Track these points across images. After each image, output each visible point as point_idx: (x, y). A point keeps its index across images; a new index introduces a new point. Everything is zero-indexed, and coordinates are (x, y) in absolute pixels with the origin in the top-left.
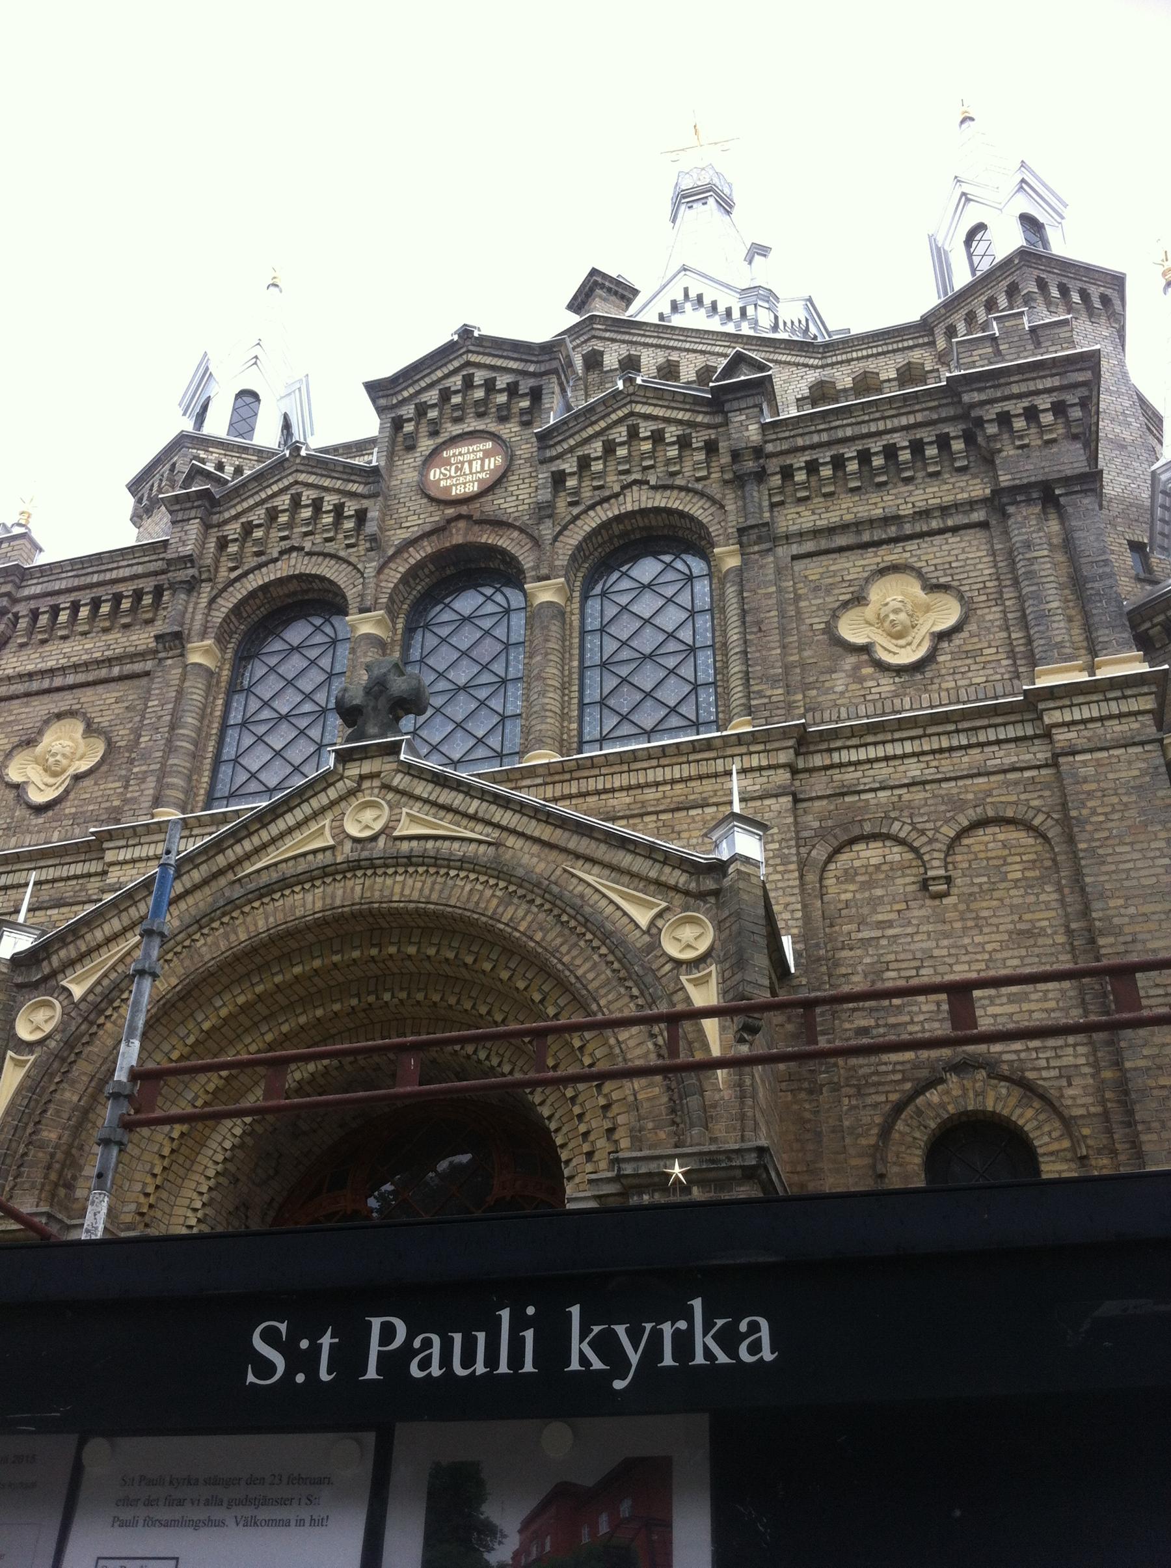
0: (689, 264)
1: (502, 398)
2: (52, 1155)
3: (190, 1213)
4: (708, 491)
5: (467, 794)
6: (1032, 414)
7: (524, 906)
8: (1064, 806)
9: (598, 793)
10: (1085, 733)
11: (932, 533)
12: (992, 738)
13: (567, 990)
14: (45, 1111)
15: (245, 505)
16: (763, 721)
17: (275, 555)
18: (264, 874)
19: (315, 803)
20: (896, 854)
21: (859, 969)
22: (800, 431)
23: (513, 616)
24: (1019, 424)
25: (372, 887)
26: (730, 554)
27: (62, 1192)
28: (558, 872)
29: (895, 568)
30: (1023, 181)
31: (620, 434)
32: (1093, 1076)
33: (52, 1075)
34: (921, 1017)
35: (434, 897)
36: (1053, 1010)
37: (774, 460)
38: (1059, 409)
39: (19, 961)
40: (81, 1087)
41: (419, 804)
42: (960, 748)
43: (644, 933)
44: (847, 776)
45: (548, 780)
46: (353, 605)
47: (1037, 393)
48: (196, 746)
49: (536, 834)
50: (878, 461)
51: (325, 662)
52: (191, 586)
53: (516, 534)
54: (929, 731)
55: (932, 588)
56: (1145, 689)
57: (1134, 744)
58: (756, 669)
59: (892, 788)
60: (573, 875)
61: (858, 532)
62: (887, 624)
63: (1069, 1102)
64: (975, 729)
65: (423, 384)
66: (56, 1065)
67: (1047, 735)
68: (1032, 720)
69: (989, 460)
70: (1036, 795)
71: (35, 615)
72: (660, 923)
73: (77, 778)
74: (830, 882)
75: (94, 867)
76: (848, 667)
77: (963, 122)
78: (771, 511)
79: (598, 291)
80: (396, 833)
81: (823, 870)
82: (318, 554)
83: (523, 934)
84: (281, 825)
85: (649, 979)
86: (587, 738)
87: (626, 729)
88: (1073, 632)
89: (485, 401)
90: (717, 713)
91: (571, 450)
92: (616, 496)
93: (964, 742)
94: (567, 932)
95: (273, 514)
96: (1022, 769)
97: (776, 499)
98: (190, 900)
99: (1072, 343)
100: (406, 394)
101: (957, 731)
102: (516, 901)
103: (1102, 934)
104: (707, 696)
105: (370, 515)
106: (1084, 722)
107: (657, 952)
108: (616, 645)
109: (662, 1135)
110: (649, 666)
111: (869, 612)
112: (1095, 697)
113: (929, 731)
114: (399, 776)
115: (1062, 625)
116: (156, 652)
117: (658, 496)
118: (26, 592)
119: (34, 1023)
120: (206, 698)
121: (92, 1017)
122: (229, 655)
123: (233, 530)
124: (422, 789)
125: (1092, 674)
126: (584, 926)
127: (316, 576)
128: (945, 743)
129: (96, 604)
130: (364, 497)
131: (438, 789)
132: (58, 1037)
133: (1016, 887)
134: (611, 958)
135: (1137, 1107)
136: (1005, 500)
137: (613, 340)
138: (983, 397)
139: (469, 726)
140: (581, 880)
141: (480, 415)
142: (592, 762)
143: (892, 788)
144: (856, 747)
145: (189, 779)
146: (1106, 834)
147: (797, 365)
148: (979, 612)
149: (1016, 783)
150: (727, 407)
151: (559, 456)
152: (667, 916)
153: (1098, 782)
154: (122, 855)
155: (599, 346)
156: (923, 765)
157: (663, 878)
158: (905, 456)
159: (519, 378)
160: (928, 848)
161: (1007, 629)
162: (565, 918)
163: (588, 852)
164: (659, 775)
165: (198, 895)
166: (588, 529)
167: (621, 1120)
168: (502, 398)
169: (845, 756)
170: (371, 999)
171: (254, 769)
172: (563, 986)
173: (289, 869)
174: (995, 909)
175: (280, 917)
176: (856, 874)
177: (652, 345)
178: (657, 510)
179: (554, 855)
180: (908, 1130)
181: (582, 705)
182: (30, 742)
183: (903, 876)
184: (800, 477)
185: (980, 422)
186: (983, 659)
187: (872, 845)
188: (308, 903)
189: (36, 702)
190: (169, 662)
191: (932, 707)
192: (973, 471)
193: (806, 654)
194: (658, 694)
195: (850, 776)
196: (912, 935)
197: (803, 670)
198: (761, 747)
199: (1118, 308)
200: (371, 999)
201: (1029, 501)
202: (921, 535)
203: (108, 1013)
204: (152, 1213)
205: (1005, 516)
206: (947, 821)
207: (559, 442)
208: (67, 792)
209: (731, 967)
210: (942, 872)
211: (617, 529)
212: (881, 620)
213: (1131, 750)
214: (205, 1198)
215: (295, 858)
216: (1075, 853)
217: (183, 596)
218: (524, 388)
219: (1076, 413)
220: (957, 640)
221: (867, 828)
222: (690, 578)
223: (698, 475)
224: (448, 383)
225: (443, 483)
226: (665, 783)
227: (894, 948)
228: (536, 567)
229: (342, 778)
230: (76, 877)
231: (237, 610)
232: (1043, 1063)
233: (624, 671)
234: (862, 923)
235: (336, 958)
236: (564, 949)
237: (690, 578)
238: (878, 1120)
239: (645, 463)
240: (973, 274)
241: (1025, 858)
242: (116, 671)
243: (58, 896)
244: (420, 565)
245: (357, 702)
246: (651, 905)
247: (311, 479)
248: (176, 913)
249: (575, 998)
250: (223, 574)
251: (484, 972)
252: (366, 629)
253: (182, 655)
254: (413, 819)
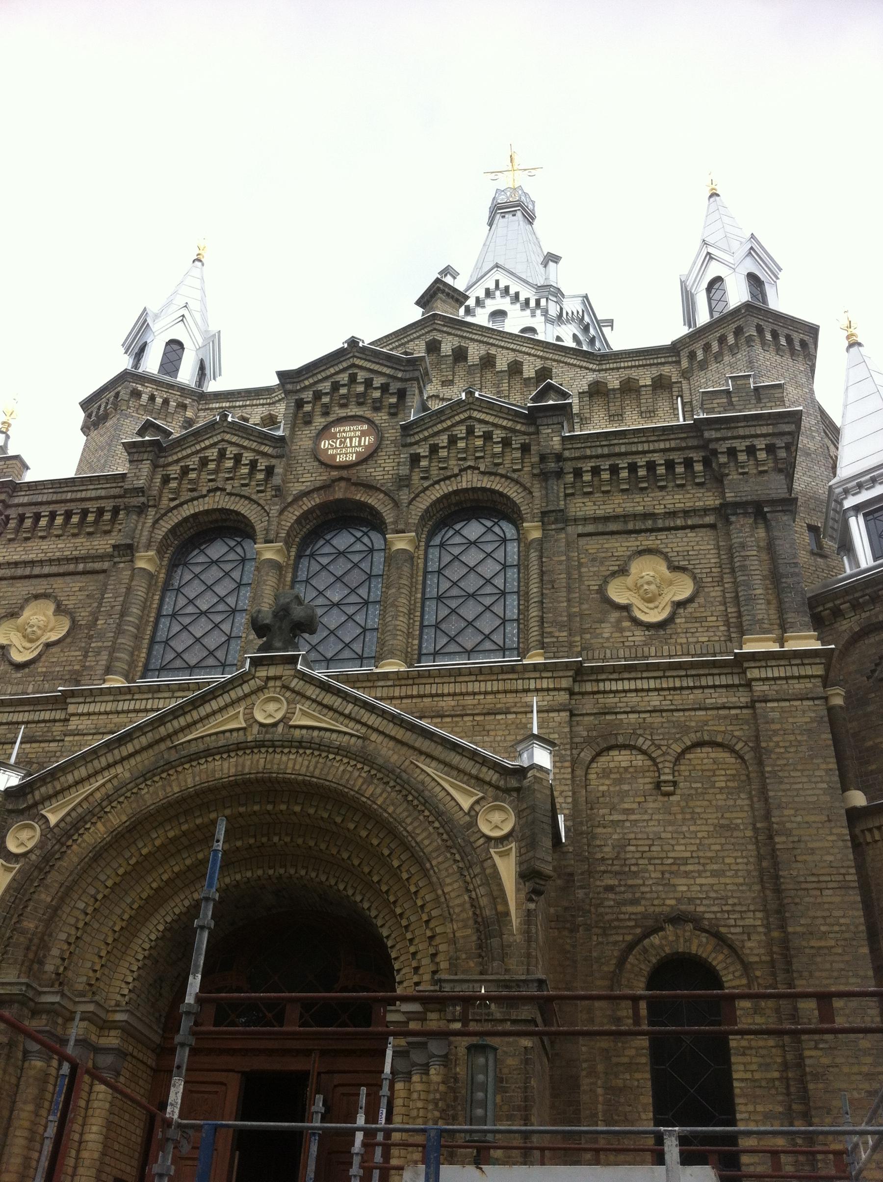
0: (500, 263)
1: (377, 394)
2: (31, 940)
3: (124, 985)
4: (522, 480)
5: (344, 699)
6: (751, 451)
7: (382, 786)
8: (757, 737)
9: (432, 696)
10: (775, 687)
11: (676, 528)
12: (710, 683)
13: (408, 849)
14: (26, 907)
15: (184, 453)
16: (552, 655)
17: (205, 492)
18: (193, 744)
19: (233, 694)
20: (639, 760)
21: (609, 842)
22: (589, 444)
23: (375, 554)
24: (742, 457)
25: (272, 761)
26: (535, 528)
27: (36, 966)
28: (407, 763)
29: (649, 551)
30: (752, 248)
31: (461, 431)
32: (765, 934)
33: (32, 881)
34: (651, 882)
35: (317, 773)
36: (742, 885)
37: (569, 463)
38: (771, 449)
39: (9, 793)
40: (53, 891)
41: (308, 703)
42: (688, 688)
43: (466, 814)
44: (608, 700)
45: (397, 683)
46: (260, 536)
47: (757, 436)
48: (138, 629)
49: (393, 734)
50: (642, 472)
51: (236, 575)
52: (141, 510)
53: (382, 496)
54: (668, 674)
55: (674, 568)
56: (818, 660)
57: (808, 699)
58: (549, 616)
59: (639, 712)
60: (417, 767)
61: (625, 522)
62: (641, 591)
63: (748, 951)
64: (699, 675)
65: (320, 377)
66: (36, 873)
67: (748, 685)
68: (739, 673)
69: (719, 480)
70: (738, 727)
71: (22, 518)
72: (477, 808)
73: (48, 645)
74: (592, 776)
75: (59, 715)
76: (612, 620)
77: (711, 196)
78: (565, 500)
79: (440, 295)
80: (291, 723)
81: (588, 768)
82: (236, 495)
83: (380, 806)
84: (207, 709)
85: (468, 849)
86: (424, 651)
87: (453, 648)
88: (771, 612)
89: (364, 395)
90: (519, 642)
91: (425, 439)
92: (456, 476)
93: (691, 684)
94: (411, 808)
95: (204, 462)
96: (730, 708)
97: (569, 491)
98: (138, 758)
99: (782, 402)
100: (307, 383)
101: (687, 676)
102: (375, 781)
103: (778, 834)
104: (512, 629)
105: (276, 470)
106: (774, 679)
107: (474, 829)
108: (448, 584)
109: (472, 964)
110: (471, 602)
111: (629, 581)
112: (782, 662)
113: (667, 674)
114: (296, 680)
115: (763, 607)
116: (112, 556)
117: (486, 479)
118: (16, 501)
119: (21, 840)
120: (147, 594)
121: (63, 839)
122: (165, 563)
123: (174, 470)
124: (311, 691)
125: (782, 641)
126: (424, 805)
127: (233, 511)
128: (678, 684)
129: (68, 515)
130: (273, 457)
131: (324, 693)
132: (38, 852)
133: (721, 793)
134: (441, 830)
135: (794, 960)
136: (729, 511)
137: (449, 334)
138: (718, 435)
139: (339, 633)
140: (423, 770)
141: (360, 404)
142: (429, 674)
143: (639, 712)
144: (616, 680)
145: (132, 654)
146: (784, 762)
147: (581, 367)
148: (706, 590)
149: (725, 717)
150: (539, 421)
151: (417, 443)
152: (483, 803)
153: (781, 723)
154: (82, 709)
155: (438, 336)
156: (661, 698)
157: (481, 776)
158: (661, 470)
159: (390, 380)
160: (662, 759)
161: (725, 604)
162: (410, 798)
163: (428, 751)
164: (476, 687)
165: (145, 755)
166: (434, 498)
167: (442, 948)
168: (377, 394)
169: (608, 686)
170: (264, 840)
171: (180, 650)
172: (405, 846)
173: (211, 743)
174: (705, 807)
175: (204, 777)
176: (611, 772)
177: (477, 341)
178: (484, 490)
179: (404, 750)
180: (636, 962)
181: (422, 627)
182: (13, 615)
183: (644, 777)
184: (587, 477)
185: (715, 453)
186: (706, 624)
187: (623, 752)
188: (225, 768)
189: (19, 584)
190: (122, 565)
191: (670, 656)
192: (708, 486)
193: (585, 606)
194: (477, 624)
195: (611, 700)
196: (647, 821)
197: (581, 618)
198: (550, 674)
199: (812, 351)
200: (264, 840)
201: (745, 514)
202: (669, 529)
203: (75, 837)
204: (97, 984)
205: (728, 523)
206: (676, 740)
207: (417, 433)
208: (40, 655)
209: (526, 846)
210: (670, 778)
211: (454, 499)
212: (637, 588)
213: (805, 703)
214: (135, 975)
215: (216, 734)
216: (762, 773)
217: (134, 517)
218: (393, 388)
219: (782, 454)
220: (690, 608)
221: (621, 740)
222: (504, 540)
223: (515, 467)
224: (338, 378)
225: (330, 452)
226: (480, 693)
227: (635, 829)
228: (395, 523)
229: (254, 678)
230: (44, 721)
231: (173, 531)
232: (732, 922)
233: (453, 604)
234: (613, 808)
235: (242, 809)
236: (409, 821)
237: (504, 540)
238: (616, 954)
239: (478, 454)
240: (711, 315)
241: (728, 772)
242: (81, 567)
243: (31, 734)
244: (311, 511)
245: (267, 621)
246: (471, 794)
247: (234, 439)
248: (127, 767)
249: (413, 856)
250: (165, 502)
251: (348, 829)
252: (268, 555)
253: (132, 561)
254: (304, 713)
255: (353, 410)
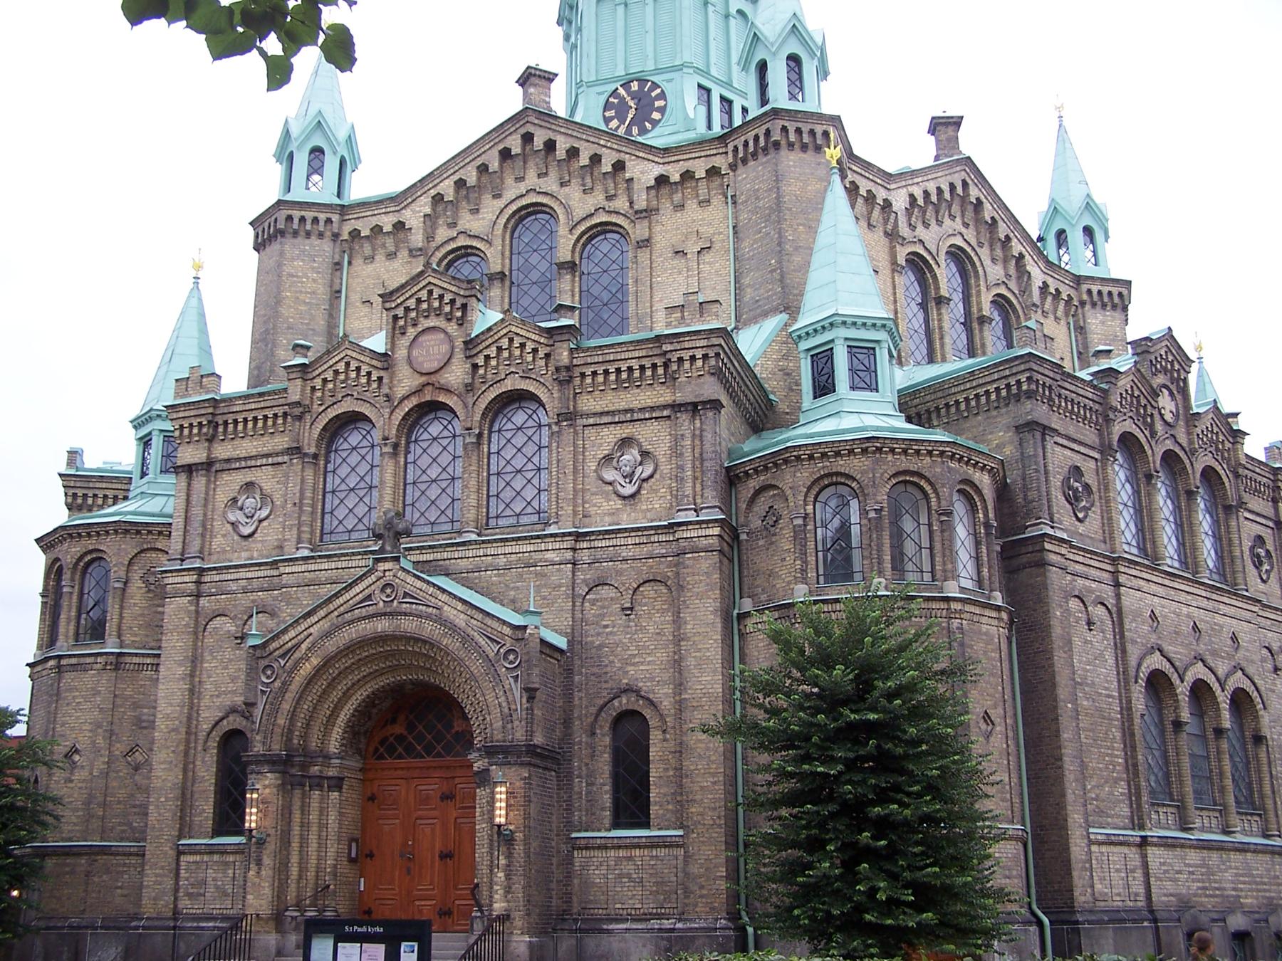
52: (300, 418)
75: (275, 573)
123: (318, 383)
154: (288, 570)
155: (531, 129)
242: (270, 460)
255: (432, 322)
